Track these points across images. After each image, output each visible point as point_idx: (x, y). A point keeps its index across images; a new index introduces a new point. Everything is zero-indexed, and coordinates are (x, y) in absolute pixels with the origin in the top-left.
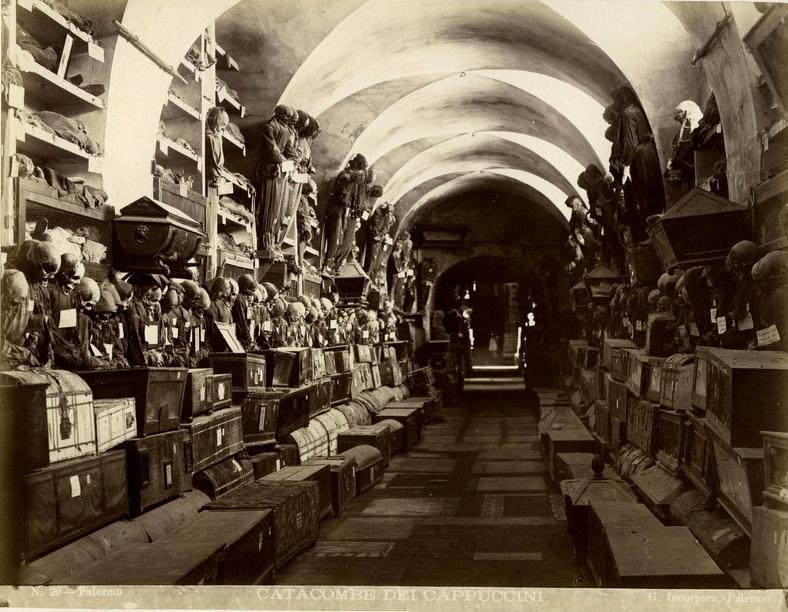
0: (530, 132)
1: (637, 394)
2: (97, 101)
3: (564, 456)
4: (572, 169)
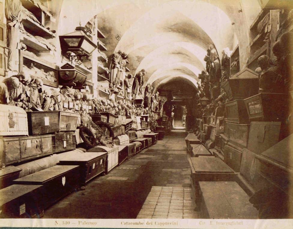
2: (54, 35)
3: (192, 145)
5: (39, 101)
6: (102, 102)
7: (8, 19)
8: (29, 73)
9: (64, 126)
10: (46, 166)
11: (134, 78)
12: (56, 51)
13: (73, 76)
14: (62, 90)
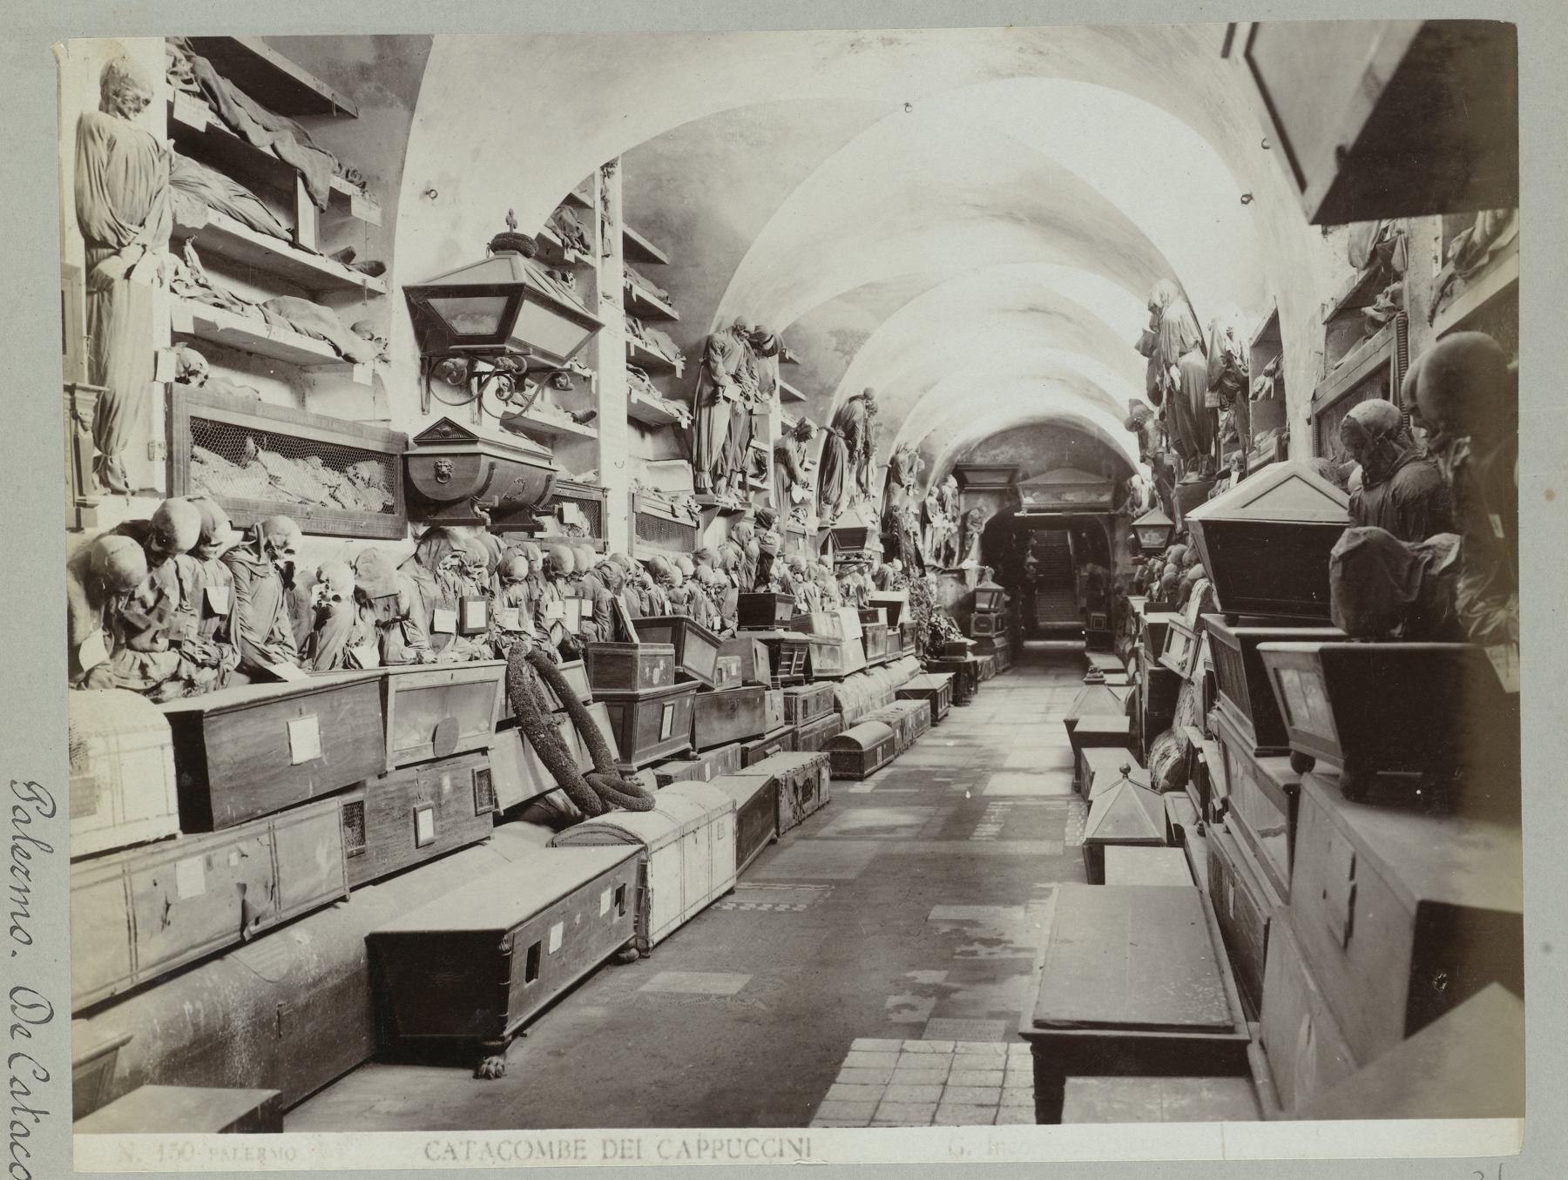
5: (286, 625)
6: (649, 566)
7: (91, 243)
8: (216, 494)
9: (417, 737)
10: (299, 968)
12: (386, 361)
13: (473, 480)
14: (424, 549)
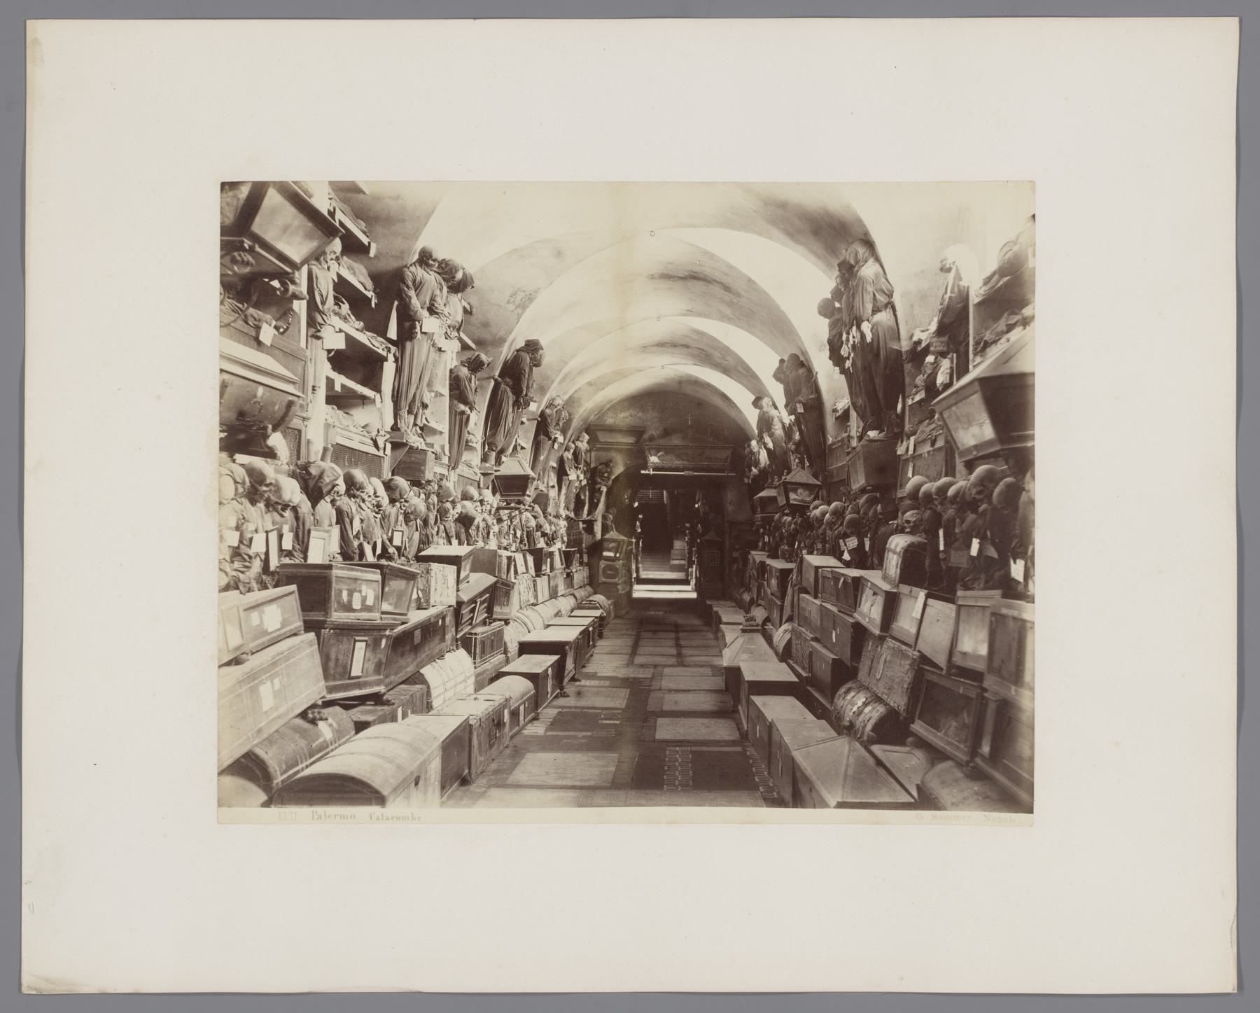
0: (723, 317)
1: (877, 632)
4: (764, 359)
11: (496, 380)
